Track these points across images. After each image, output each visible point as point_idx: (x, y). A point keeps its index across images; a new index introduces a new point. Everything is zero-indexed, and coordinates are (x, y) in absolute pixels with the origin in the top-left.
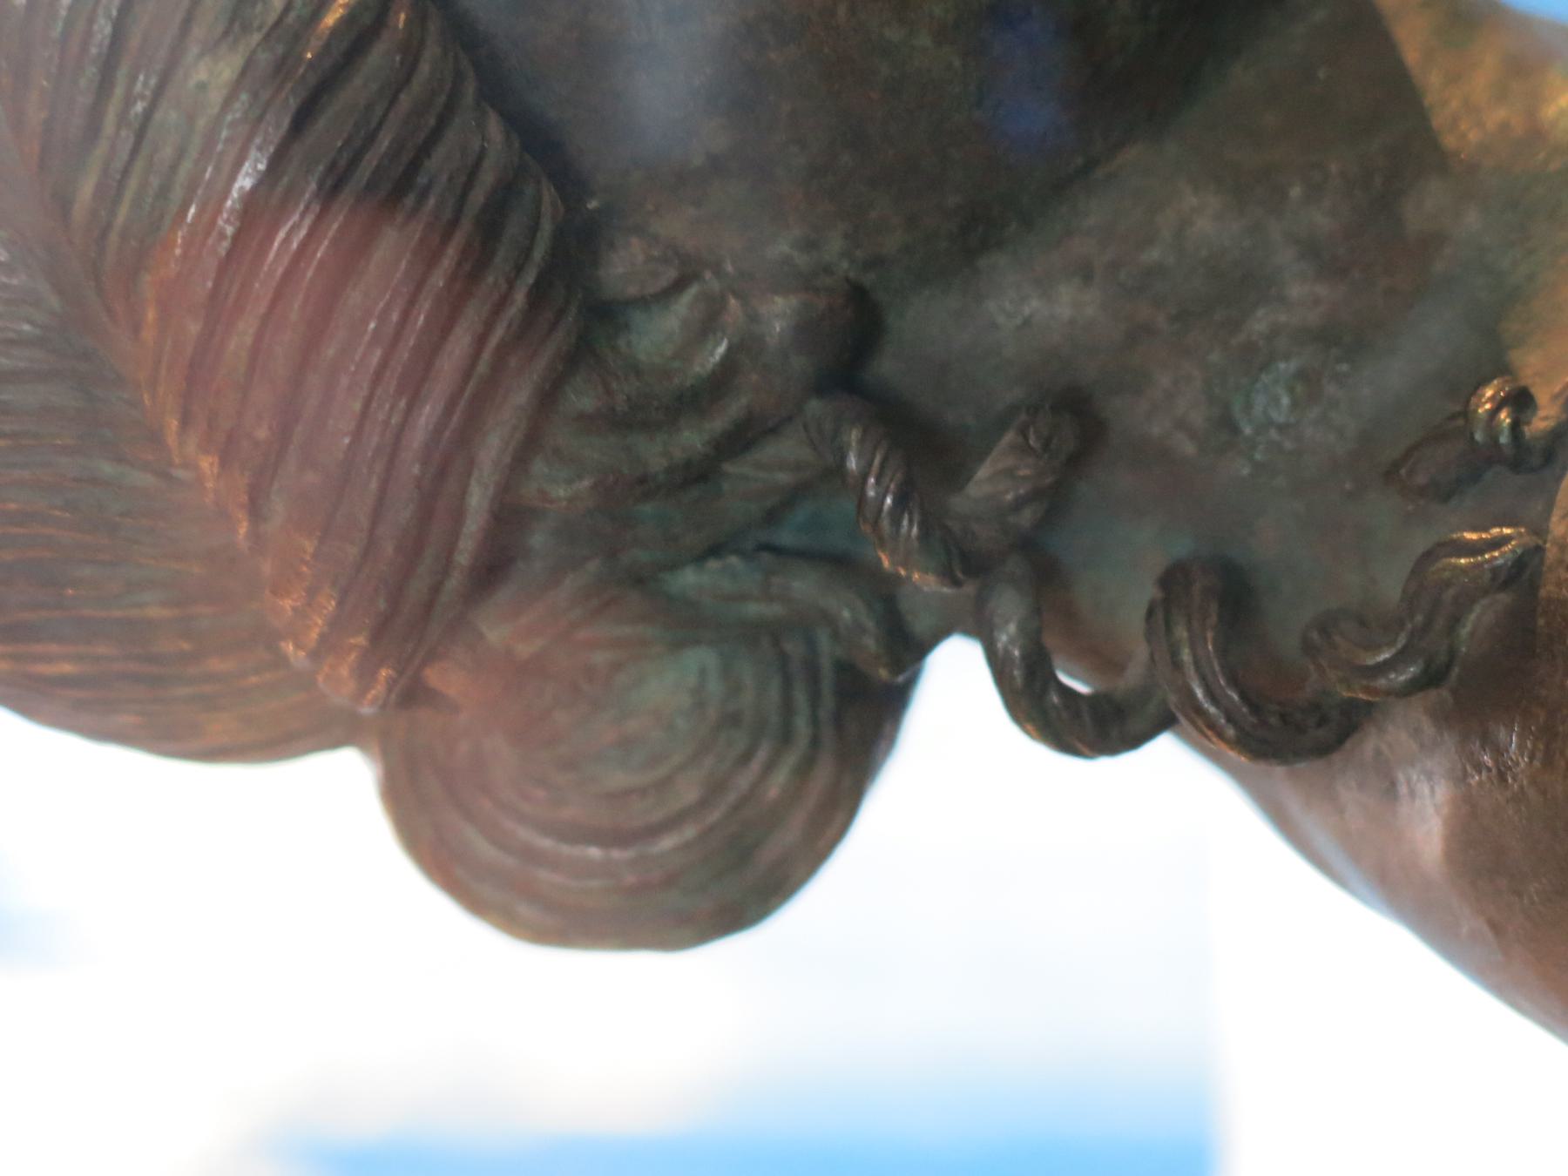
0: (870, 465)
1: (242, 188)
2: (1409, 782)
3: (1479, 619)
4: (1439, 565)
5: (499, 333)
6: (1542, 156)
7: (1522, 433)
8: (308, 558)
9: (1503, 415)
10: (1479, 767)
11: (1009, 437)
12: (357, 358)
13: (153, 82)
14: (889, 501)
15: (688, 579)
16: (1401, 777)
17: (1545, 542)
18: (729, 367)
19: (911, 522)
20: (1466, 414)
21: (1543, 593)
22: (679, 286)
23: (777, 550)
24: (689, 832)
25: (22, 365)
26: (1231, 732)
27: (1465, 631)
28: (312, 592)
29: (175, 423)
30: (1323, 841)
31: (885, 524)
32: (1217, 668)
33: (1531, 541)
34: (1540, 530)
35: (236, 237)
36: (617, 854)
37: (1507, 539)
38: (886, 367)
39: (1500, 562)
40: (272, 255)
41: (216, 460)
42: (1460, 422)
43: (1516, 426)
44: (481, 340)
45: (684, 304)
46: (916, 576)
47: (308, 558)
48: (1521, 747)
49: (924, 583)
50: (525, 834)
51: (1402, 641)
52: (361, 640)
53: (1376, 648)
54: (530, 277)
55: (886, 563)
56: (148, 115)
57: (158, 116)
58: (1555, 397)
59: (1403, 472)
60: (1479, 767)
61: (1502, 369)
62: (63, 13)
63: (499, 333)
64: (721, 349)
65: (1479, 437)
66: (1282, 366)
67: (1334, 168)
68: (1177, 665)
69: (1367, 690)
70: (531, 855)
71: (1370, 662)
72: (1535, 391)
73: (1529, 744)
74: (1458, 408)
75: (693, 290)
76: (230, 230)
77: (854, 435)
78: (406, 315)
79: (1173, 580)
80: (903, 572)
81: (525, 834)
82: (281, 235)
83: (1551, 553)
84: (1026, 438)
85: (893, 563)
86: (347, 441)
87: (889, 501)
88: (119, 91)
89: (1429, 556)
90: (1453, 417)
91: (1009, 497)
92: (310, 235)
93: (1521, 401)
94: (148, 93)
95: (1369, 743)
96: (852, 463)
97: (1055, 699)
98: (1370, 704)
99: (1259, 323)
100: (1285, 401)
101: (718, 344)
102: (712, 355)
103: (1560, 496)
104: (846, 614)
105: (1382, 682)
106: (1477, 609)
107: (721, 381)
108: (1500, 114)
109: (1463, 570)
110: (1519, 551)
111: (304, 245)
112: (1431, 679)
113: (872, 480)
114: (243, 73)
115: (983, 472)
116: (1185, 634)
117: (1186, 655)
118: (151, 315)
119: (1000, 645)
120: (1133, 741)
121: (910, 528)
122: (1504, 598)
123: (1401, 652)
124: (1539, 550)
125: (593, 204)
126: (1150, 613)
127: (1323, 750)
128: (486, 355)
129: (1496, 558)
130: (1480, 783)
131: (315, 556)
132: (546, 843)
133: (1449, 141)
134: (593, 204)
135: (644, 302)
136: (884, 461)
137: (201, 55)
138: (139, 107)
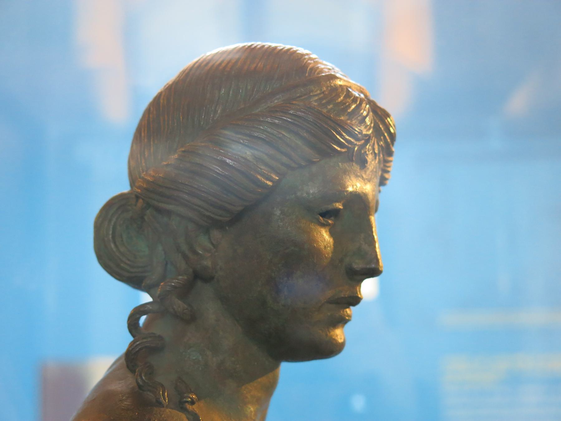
0: (179, 280)
1: (227, 160)
2: (122, 383)
3: (150, 396)
4: (161, 388)
5: (202, 210)
6: (241, 405)
7: (186, 403)
8: (159, 175)
9: (189, 399)
10: (123, 396)
11: (186, 306)
12: (195, 183)
13: (246, 144)
14: (173, 284)
15: (160, 248)
16: (123, 381)
17: (165, 408)
18: (198, 254)
19: (169, 288)
20: (191, 392)
21: (155, 408)
22: (212, 244)
23: (167, 264)
24: (115, 249)
25: (195, 123)
26: (131, 349)
27: (149, 393)
28: (153, 176)
29: (183, 150)
30: (114, 367)
31: (169, 284)
32: (142, 346)
33: (165, 406)
34: (167, 407)
35: (217, 159)
36: (110, 236)
37: (165, 401)
38: (199, 283)
39: (161, 400)
40: (214, 166)
41: (177, 157)
42: (189, 391)
43: (187, 402)
44: (199, 206)
45: (209, 246)
46: (159, 290)
47: (159, 175)
48: (125, 404)
49: (158, 291)
50: (114, 219)
51: (146, 381)
52: (145, 186)
53: (145, 376)
54: (212, 216)
55: (162, 284)
56: (241, 143)
57: (240, 145)
58: (194, 409)
59: (180, 380)
60: (123, 396)
61: (199, 399)
62: (259, 127)
63: (202, 210)
64: (201, 252)
65: (185, 395)
66: (201, 357)
67: (238, 366)
68: (143, 339)
69: (137, 375)
70: (110, 221)
71: (143, 375)
72: (195, 405)
73: (126, 406)
74: (192, 390)
75: (212, 247)
76: (219, 158)
77: (186, 278)
78: (204, 192)
79: (160, 338)
80: (160, 287)
81: (114, 219)
82: (217, 167)
83: (162, 409)
84: (186, 310)
85: (162, 285)
86: (180, 181)
87: (173, 284)
88: (245, 138)
89: (162, 386)
90: (191, 390)
91: (175, 307)
92: (218, 173)
93: (193, 403)
94: (244, 143)
95: (130, 375)
96: (180, 277)
97: (138, 316)
98: (135, 375)
99: (209, 353)
100: (194, 358)
101: (202, 252)
102: (200, 251)
103: (174, 410)
104: (154, 277)
105: (139, 377)
106: (153, 395)
107: (195, 252)
108: (249, 397)
109: (159, 393)
110: (163, 403)
111: (216, 172)
112: (140, 387)
113: (177, 281)
114: (248, 160)
115: (180, 302)
116: (149, 340)
117: (145, 340)
118: (203, 144)
119: (147, 305)
120: (130, 331)
121: (168, 288)
122: (154, 400)
123: (144, 381)
124: (163, 407)
125: (227, 228)
126: (154, 334)
127: (128, 367)
128: (197, 207)
129: (162, 398)
130: (120, 396)
131: (160, 176)
132: (112, 223)
133: (243, 387)
134: (227, 228)
135: (210, 238)
136: (180, 283)
137: (252, 153)
138: (242, 141)
